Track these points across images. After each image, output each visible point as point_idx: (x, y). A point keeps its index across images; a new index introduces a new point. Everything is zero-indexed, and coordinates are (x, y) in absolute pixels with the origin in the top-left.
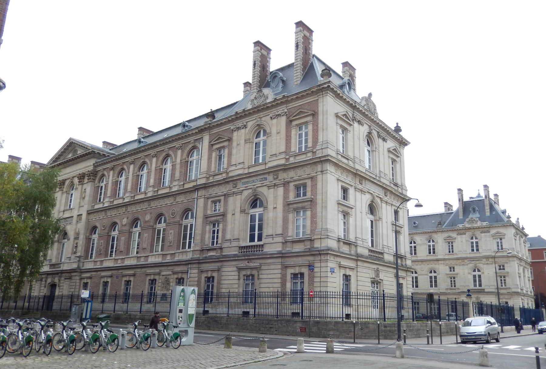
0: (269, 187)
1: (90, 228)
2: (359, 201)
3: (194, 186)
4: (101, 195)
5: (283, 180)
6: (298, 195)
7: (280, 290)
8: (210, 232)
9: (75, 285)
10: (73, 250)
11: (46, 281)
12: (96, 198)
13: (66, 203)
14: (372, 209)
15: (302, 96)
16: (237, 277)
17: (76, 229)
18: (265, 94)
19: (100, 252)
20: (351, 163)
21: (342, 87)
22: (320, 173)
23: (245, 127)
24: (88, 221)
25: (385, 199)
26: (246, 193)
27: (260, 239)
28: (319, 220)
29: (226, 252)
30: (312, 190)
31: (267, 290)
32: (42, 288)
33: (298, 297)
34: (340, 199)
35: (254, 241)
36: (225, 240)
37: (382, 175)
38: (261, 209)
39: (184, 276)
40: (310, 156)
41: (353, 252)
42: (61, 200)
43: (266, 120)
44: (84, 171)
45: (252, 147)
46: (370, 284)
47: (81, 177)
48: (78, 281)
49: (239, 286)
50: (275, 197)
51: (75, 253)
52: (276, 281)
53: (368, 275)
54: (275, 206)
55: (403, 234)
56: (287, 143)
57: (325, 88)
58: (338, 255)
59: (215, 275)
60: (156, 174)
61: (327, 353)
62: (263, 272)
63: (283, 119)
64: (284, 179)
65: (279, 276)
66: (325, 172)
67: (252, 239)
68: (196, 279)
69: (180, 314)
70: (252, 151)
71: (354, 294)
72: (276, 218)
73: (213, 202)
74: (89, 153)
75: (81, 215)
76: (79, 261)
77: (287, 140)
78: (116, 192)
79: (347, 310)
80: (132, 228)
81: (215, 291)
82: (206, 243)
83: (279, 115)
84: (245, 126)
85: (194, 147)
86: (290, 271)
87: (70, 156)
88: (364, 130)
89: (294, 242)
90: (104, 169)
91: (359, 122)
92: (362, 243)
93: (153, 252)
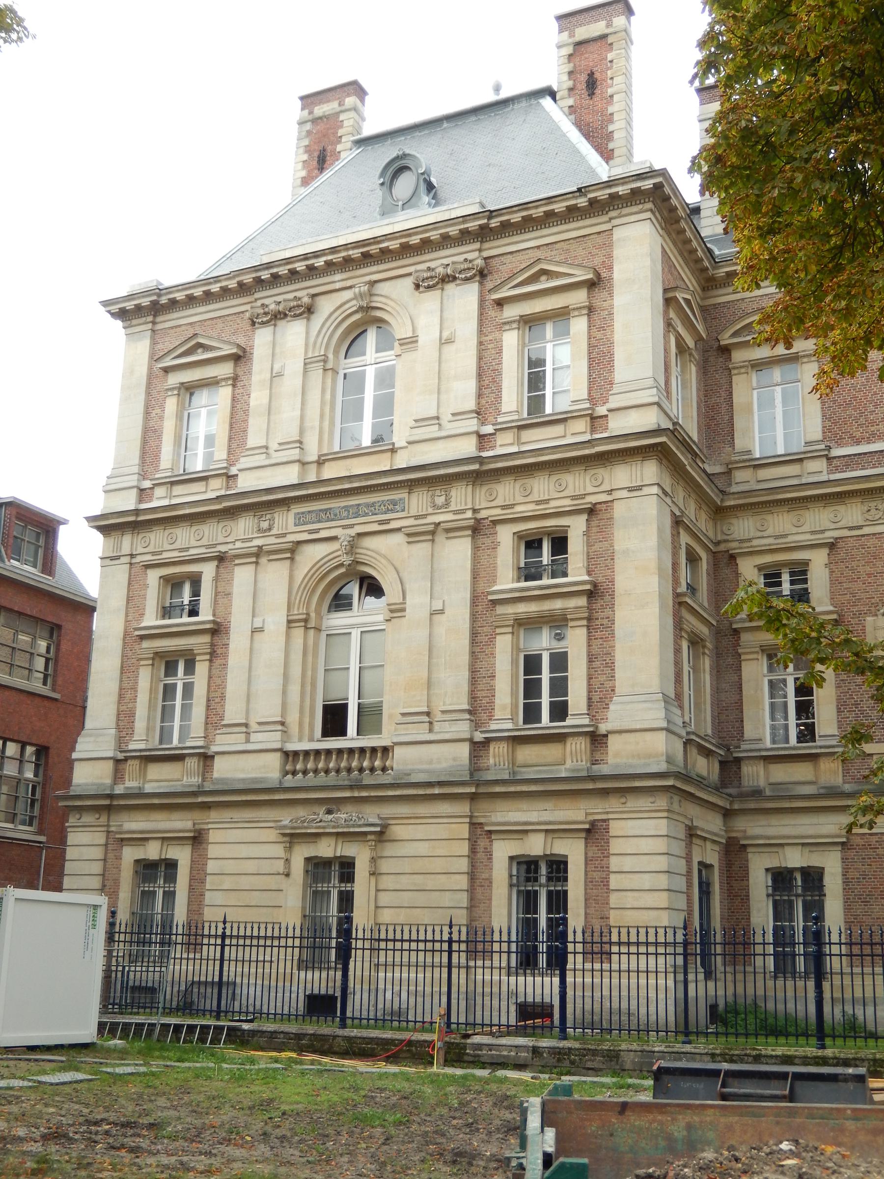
0: (413, 536)
5: (469, 514)
6: (530, 573)
15: (550, 215)
26: (314, 554)
29: (225, 770)
35: (342, 732)
40: (216, 489)
43: (397, 294)
59: (182, 855)
64: (475, 511)
73: (165, 579)
81: (180, 914)
86: (130, 855)
89: (148, 759)
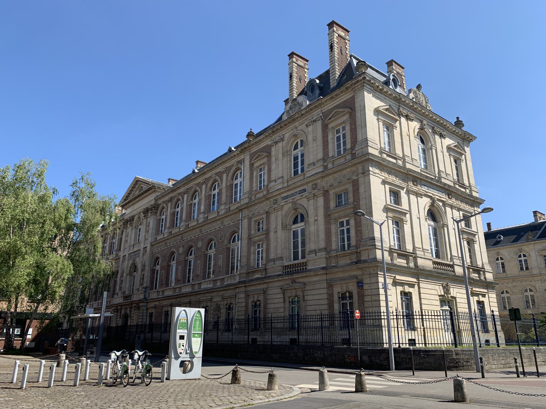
1: (154, 259)
2: (417, 206)
3: (238, 208)
4: (162, 227)
7: (326, 312)
8: (254, 253)
9: (143, 316)
10: (140, 282)
11: (121, 313)
12: (158, 231)
13: (135, 237)
14: (433, 215)
16: (282, 300)
17: (142, 262)
18: (300, 102)
19: (162, 282)
20: (400, 163)
21: (387, 83)
22: (361, 175)
23: (282, 140)
24: (151, 251)
25: (450, 202)
27: (303, 257)
28: (364, 229)
30: (354, 196)
31: (314, 313)
32: (118, 319)
33: (347, 321)
34: (389, 203)
36: (268, 260)
37: (443, 175)
38: (303, 224)
39: (233, 301)
41: (412, 265)
42: (131, 235)
44: (148, 205)
45: (290, 161)
46: (438, 303)
47: (146, 211)
48: (145, 311)
49: (285, 310)
50: (316, 209)
51: (142, 284)
52: (322, 302)
53: (434, 292)
54: (316, 218)
55: (478, 242)
56: (324, 149)
57: (361, 80)
58: (392, 269)
60: (205, 200)
61: (356, 392)
62: (309, 293)
63: (319, 124)
65: (325, 296)
66: (366, 174)
67: (296, 258)
68: (244, 304)
69: (182, 342)
70: (291, 165)
71: (417, 314)
72: (318, 231)
74: (151, 188)
75: (146, 247)
76: (145, 291)
77: (324, 146)
78: (174, 223)
79: (412, 335)
80: (187, 256)
82: (252, 265)
83: (315, 121)
84: (282, 139)
85: (238, 169)
87: (137, 193)
88: (415, 125)
90: (164, 202)
91: (407, 117)
92: (423, 253)
93: (205, 279)
